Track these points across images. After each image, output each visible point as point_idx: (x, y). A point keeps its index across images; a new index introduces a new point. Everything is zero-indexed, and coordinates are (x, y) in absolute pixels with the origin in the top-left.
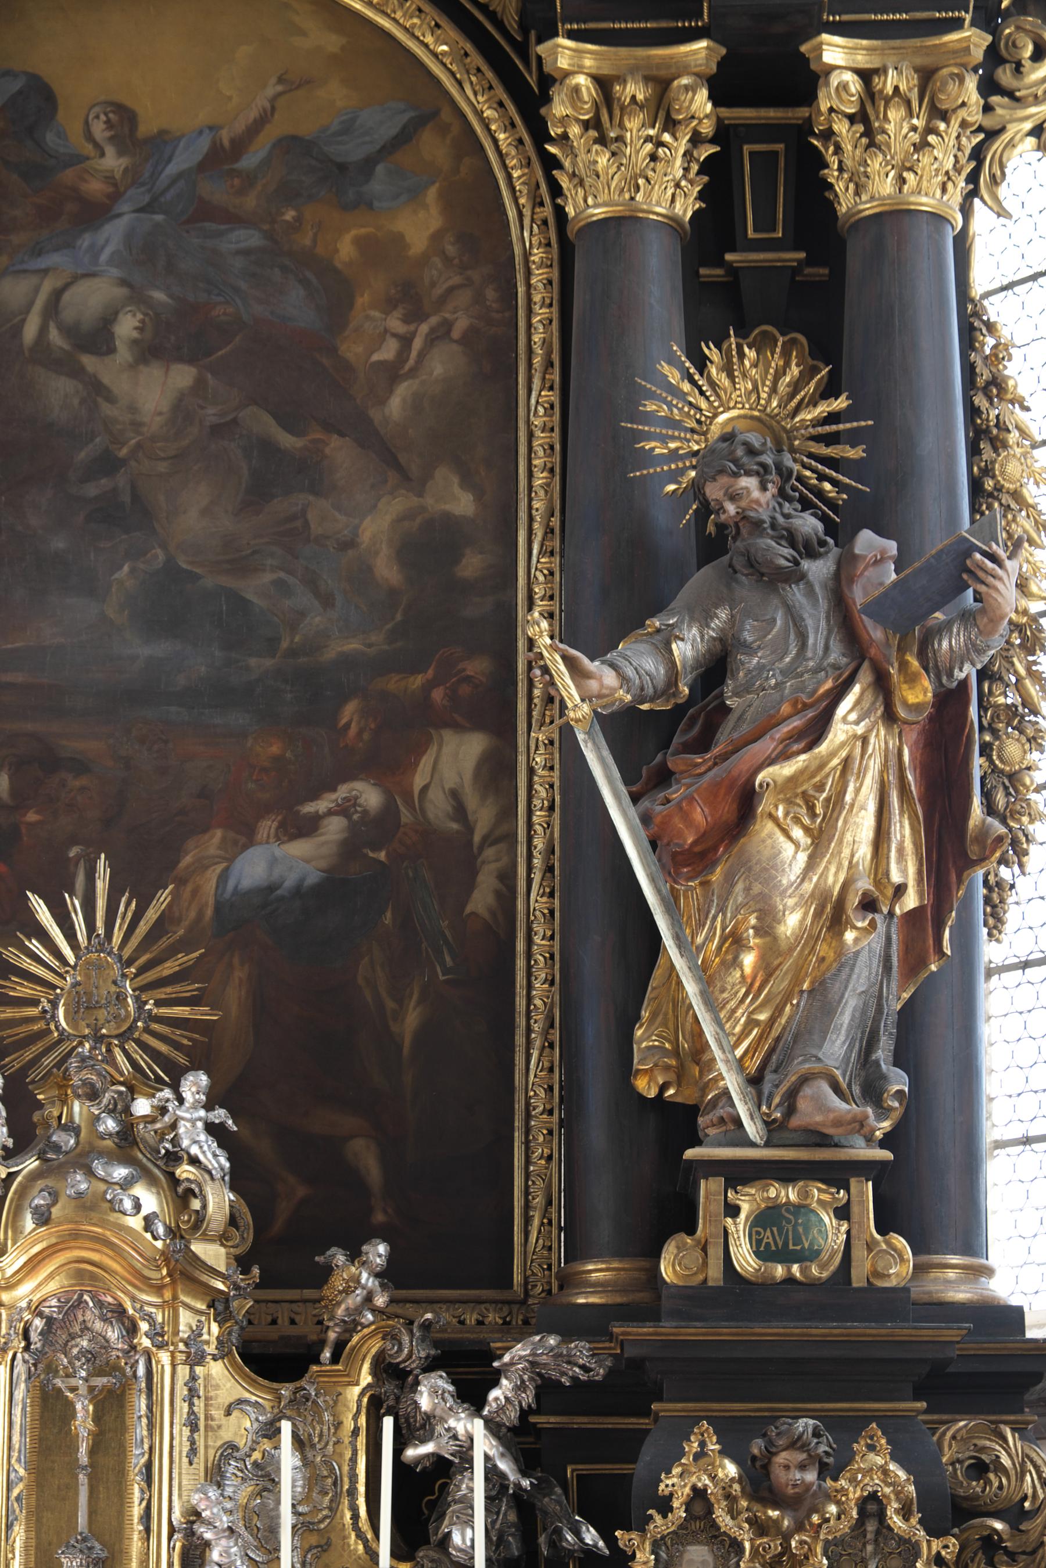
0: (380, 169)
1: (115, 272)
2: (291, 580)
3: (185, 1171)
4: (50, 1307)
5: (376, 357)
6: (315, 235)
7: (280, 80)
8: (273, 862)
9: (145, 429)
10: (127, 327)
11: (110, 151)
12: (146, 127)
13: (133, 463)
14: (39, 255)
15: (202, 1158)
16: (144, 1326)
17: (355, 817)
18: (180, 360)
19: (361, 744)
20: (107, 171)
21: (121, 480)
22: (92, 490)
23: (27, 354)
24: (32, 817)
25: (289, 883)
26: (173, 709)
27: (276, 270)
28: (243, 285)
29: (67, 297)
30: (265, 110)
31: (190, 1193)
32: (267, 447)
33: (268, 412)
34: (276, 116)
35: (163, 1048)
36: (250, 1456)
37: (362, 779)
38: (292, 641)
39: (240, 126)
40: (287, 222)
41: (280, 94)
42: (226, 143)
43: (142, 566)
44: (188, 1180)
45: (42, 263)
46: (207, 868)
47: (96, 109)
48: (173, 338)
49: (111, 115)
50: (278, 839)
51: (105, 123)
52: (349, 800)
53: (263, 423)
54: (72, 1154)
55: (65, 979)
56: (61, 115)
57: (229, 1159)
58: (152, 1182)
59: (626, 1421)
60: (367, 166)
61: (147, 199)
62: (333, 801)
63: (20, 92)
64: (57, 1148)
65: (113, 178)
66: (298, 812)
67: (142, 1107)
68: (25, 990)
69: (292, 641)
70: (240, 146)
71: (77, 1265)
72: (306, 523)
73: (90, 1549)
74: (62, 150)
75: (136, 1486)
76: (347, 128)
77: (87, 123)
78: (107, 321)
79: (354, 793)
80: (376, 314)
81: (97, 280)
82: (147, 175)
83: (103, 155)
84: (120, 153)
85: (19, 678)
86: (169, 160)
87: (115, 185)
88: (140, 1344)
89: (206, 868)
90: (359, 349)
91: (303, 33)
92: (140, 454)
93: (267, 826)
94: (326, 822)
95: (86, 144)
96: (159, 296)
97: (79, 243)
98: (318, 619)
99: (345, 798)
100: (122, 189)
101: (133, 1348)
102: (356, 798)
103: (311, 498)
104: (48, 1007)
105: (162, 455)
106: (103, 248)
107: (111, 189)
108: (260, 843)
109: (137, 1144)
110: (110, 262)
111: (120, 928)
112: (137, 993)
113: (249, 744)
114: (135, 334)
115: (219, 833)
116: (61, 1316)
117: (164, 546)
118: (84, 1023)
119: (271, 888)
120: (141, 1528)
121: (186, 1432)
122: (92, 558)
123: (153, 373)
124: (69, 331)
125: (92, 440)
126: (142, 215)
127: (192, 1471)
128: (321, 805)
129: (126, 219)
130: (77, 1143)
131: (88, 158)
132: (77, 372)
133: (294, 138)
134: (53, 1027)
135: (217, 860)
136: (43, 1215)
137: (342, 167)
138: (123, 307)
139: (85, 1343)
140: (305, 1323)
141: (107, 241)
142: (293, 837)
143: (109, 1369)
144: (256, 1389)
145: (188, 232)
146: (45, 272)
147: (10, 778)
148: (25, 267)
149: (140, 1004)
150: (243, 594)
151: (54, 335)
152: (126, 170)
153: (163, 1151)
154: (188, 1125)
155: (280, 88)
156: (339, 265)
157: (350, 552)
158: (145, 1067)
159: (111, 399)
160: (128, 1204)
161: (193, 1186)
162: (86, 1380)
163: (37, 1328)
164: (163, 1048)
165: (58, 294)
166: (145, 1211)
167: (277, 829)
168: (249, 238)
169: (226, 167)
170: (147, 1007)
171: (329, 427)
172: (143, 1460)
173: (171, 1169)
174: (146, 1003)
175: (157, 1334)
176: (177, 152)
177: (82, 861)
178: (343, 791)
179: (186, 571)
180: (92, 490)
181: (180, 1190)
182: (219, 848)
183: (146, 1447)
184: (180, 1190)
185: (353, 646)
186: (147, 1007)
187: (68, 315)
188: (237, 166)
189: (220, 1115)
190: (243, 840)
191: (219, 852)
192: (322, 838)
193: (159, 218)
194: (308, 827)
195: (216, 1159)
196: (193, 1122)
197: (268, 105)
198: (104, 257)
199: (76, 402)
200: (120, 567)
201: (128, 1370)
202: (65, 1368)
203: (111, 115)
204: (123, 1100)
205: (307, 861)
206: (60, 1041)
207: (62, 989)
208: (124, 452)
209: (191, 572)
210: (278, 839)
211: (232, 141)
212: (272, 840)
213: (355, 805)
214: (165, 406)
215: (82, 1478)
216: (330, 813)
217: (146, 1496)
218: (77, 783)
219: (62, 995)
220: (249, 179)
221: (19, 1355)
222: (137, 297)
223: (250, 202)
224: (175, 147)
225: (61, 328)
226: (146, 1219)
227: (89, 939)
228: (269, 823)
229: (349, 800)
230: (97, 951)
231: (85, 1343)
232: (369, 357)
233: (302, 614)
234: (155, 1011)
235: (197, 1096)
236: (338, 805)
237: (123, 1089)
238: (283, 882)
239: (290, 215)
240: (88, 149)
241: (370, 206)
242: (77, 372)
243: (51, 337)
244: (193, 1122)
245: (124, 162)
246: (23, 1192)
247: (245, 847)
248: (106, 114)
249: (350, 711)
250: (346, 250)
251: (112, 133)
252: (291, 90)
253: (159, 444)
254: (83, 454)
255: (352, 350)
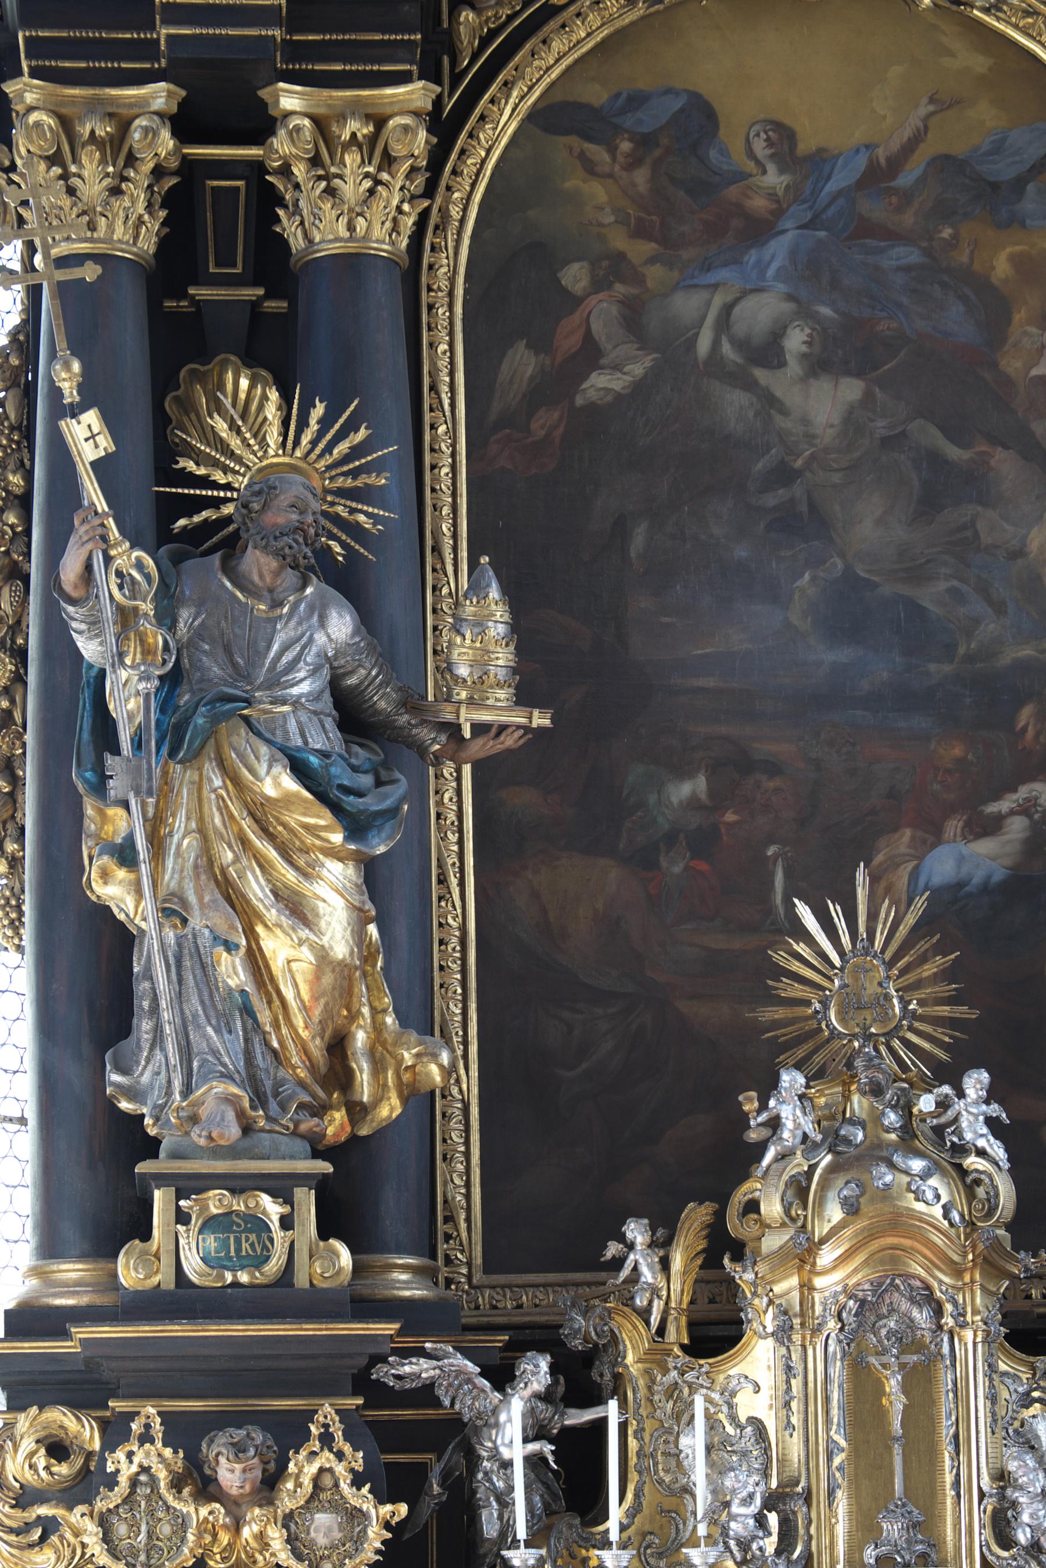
0: (1031, 187)
1: (782, 287)
2: (965, 588)
3: (972, 1162)
4: (863, 1290)
5: (1034, 372)
6: (972, 252)
7: (932, 100)
8: (961, 860)
9: (818, 441)
10: (796, 341)
11: (771, 168)
12: (805, 146)
13: (808, 474)
14: (708, 270)
15: (988, 1149)
16: (949, 1307)
17: (1036, 816)
18: (848, 373)
19: (1038, 747)
20: (769, 188)
21: (798, 490)
22: (771, 500)
23: (701, 366)
24: (730, 817)
25: (978, 878)
26: (858, 712)
27: (936, 286)
28: (905, 300)
29: (737, 310)
30: (918, 130)
31: (978, 1182)
32: (935, 459)
33: (936, 426)
34: (929, 136)
35: (926, 1045)
36: (1012, 1425)
37: (1041, 780)
38: (969, 647)
39: (895, 145)
40: (944, 239)
41: (931, 114)
42: (883, 161)
43: (822, 574)
44: (977, 1171)
45: (712, 278)
46: (898, 865)
47: (756, 128)
48: (840, 352)
49: (770, 133)
50: (965, 838)
51: (765, 140)
52: (1029, 801)
53: (934, 437)
54: (863, 1147)
55: (833, 981)
56: (722, 132)
57: (1006, 1150)
58: (944, 1173)
59: (250, 1402)
60: (1019, 185)
61: (809, 215)
62: (1014, 802)
63: (682, 110)
64: (847, 1141)
65: (776, 195)
66: (983, 811)
67: (926, 1103)
68: (798, 991)
69: (969, 647)
70: (896, 164)
71: (880, 1254)
72: (976, 535)
73: (909, 1513)
74: (725, 167)
75: (947, 1455)
76: (998, 148)
77: (748, 140)
78: (777, 335)
79: (1034, 793)
80: (1034, 330)
81: (765, 295)
82: (808, 192)
83: (764, 172)
84: (782, 171)
85: (710, 682)
86: (829, 178)
87: (778, 202)
88: (947, 1324)
89: (898, 865)
90: (1018, 364)
91: (952, 54)
92: (815, 465)
93: (954, 826)
94: (1009, 821)
95: (749, 162)
96: (825, 311)
97: (746, 258)
98: (992, 626)
99: (1024, 799)
100: (785, 206)
101: (940, 1327)
102: (1036, 798)
103: (979, 509)
104: (818, 1006)
105: (835, 466)
106: (769, 264)
107: (774, 206)
108: (948, 842)
109: (917, 1137)
110: (777, 277)
111: (882, 933)
112: (901, 993)
113: (932, 747)
114: (804, 348)
115: (908, 833)
116: (874, 1299)
117: (842, 555)
118: (853, 1023)
119: (960, 885)
120: (953, 1493)
121: (988, 1404)
122: (774, 566)
123: (823, 386)
124: (741, 345)
125: (768, 451)
126: (805, 231)
127: (994, 1440)
128: (1004, 805)
129: (790, 235)
130: (865, 1136)
131: (751, 176)
132: (750, 385)
133: (947, 157)
134: (824, 1027)
135: (907, 858)
136: (852, 1205)
137: (995, 186)
138: (791, 322)
139: (892, 1324)
140: (1015, 1297)
141: (773, 257)
142: (978, 836)
143: (918, 1346)
144: (1013, 1362)
145: (850, 248)
146: (715, 286)
147: (707, 780)
148: (695, 281)
149: (905, 1003)
150: (919, 602)
151: (727, 348)
152: (787, 187)
153: (949, 1144)
154: (971, 1118)
155: (931, 108)
156: (994, 280)
157: (1019, 561)
158: (909, 1063)
159: (784, 412)
160: (929, 1195)
161: (983, 1177)
162: (898, 1358)
163: (851, 1310)
164: (926, 1045)
165: (728, 309)
166: (943, 1201)
167: (963, 829)
168: (909, 255)
169: (884, 185)
170: (911, 1007)
171: (994, 440)
172: (952, 1431)
173: (958, 1161)
174: (909, 1002)
175: (960, 1314)
176: (836, 171)
177: (780, 859)
178: (1023, 792)
179: (864, 579)
180: (771, 500)
181: (969, 1180)
182: (909, 847)
183: (953, 1418)
184: (969, 1180)
185: (1027, 652)
186: (911, 1007)
187: (740, 328)
188: (893, 184)
189: (994, 1109)
190: (931, 839)
191: (908, 851)
192: (1006, 837)
193: (822, 234)
194: (991, 827)
195: (999, 1151)
196: (976, 1116)
197: (921, 125)
198: (770, 273)
199: (751, 414)
200: (802, 575)
201: (933, 1346)
202: (876, 1346)
203: (770, 133)
204: (906, 1096)
205: (993, 859)
206: (828, 1041)
207: (830, 991)
208: (799, 463)
209: (869, 580)
210: (965, 838)
211: (888, 159)
212: (958, 839)
213: (1035, 805)
214: (836, 419)
215: (897, 1450)
216: (1012, 813)
217: (956, 1464)
218: (771, 784)
219: (832, 996)
220: (906, 197)
221: (833, 1335)
222: (804, 313)
223: (908, 219)
224: (835, 164)
225: (733, 341)
226: (944, 1207)
227: (854, 944)
228: (955, 822)
229: (1029, 801)
230: (862, 955)
231: (892, 1324)
232: (1029, 372)
233: (977, 621)
234: (920, 1011)
235: (981, 1093)
236: (1019, 805)
237: (906, 1085)
238: (971, 880)
239: (947, 233)
240: (751, 166)
241: (1023, 225)
242: (750, 385)
243: (724, 351)
244: (976, 1116)
245: (785, 179)
246: (825, 1185)
247: (934, 846)
248: (766, 132)
249: (1026, 715)
250: (1002, 267)
251: (773, 151)
252: (941, 110)
253: (833, 456)
254: (760, 466)
255: (1012, 365)
